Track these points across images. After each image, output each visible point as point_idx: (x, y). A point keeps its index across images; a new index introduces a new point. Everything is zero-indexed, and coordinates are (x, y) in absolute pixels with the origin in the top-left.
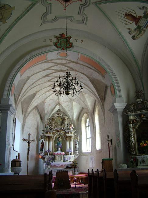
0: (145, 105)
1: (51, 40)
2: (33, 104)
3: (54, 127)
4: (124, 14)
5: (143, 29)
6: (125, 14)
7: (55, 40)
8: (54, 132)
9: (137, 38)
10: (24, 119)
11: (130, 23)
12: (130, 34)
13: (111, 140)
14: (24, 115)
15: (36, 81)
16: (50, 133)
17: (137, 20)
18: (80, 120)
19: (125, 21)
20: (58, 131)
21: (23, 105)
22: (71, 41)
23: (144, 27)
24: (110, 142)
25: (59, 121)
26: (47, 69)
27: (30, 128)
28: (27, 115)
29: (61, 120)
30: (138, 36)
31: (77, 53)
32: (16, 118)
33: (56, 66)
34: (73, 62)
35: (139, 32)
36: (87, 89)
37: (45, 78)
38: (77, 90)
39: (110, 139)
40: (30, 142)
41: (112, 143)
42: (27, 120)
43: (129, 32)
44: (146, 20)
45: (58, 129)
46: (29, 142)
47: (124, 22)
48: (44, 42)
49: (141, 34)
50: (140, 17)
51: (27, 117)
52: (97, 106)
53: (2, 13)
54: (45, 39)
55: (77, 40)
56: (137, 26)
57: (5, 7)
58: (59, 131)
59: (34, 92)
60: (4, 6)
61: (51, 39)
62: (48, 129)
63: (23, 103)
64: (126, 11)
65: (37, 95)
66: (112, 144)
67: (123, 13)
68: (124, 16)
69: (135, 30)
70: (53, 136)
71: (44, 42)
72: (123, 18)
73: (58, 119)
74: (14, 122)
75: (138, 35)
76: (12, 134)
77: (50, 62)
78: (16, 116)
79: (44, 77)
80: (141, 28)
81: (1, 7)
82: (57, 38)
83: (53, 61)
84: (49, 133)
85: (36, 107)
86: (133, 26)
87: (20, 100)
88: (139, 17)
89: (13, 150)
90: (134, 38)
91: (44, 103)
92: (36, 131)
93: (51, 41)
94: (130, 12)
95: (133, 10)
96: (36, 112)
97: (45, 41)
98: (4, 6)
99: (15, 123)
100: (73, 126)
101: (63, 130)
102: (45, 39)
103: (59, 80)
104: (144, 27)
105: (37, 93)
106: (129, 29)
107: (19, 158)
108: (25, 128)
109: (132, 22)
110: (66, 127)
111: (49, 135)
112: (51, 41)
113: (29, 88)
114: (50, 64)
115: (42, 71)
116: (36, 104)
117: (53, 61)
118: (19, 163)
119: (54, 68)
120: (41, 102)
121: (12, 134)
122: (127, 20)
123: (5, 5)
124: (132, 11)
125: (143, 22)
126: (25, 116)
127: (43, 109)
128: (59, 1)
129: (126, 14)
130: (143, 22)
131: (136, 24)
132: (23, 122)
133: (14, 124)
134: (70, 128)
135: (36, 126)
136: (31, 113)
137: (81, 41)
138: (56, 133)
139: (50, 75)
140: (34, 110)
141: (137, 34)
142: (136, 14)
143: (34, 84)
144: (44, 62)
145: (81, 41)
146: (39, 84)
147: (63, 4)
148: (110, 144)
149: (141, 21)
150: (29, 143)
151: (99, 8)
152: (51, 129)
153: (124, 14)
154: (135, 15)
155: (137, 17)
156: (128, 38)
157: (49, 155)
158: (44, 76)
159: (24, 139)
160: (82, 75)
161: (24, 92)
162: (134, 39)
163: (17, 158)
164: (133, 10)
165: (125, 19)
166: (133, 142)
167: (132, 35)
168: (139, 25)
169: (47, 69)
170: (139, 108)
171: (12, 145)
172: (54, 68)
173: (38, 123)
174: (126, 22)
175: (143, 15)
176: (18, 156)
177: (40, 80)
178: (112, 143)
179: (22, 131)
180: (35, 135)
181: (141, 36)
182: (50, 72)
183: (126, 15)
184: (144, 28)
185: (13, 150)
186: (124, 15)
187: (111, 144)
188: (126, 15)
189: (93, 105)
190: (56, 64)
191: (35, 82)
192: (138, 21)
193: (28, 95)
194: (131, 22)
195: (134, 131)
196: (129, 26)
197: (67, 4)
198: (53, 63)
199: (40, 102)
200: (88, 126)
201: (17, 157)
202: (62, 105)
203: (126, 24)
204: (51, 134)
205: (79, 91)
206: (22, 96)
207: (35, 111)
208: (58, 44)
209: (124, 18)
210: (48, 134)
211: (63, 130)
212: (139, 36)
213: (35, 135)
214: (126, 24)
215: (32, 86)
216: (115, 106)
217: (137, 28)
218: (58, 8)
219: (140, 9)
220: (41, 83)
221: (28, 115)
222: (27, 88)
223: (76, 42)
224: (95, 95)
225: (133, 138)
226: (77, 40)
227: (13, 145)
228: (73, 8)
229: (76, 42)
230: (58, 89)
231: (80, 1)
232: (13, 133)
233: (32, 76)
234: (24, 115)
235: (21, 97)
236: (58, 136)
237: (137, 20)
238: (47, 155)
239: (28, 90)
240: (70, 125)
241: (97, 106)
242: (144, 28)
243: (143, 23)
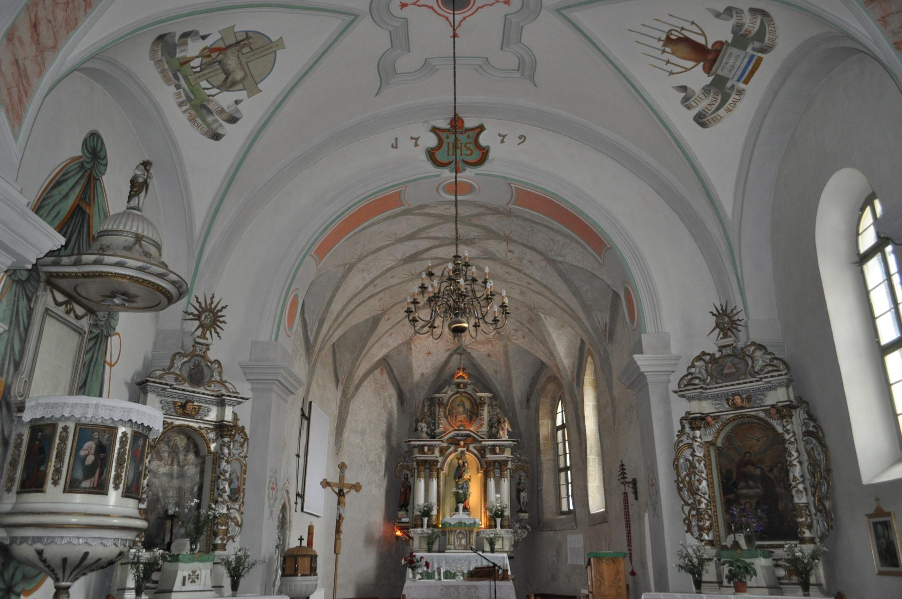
0: (750, 362)
1: (417, 139)
2: (371, 352)
3: (444, 428)
4: (659, 40)
5: (733, 86)
6: (663, 37)
7: (431, 141)
8: (445, 445)
9: (716, 120)
10: (341, 402)
11: (687, 70)
12: (689, 108)
13: (634, 482)
14: (341, 388)
15: (376, 278)
16: (431, 449)
17: (710, 57)
18: (533, 404)
19: (668, 62)
20: (457, 444)
21: (337, 356)
22: (483, 140)
23: (738, 80)
24: (630, 490)
25: (461, 409)
26: (411, 237)
27: (363, 433)
28: (352, 389)
29: (468, 405)
30: (719, 112)
31: (413, 204)
32: (311, 403)
33: (439, 224)
34: (496, 211)
35: (720, 98)
36: (551, 300)
37: (406, 267)
38: (489, 319)
39: (629, 479)
40: (345, 491)
41: (636, 493)
42: (352, 406)
43: (685, 100)
44: (742, 56)
45: (458, 435)
46: (341, 491)
47: (662, 65)
48: (393, 147)
49: (727, 105)
50: (720, 45)
51: (353, 396)
52: (590, 359)
53: (244, 61)
54: (396, 139)
55: (504, 136)
56: (711, 78)
57: (251, 41)
58: (462, 443)
59: (374, 313)
60: (248, 38)
61: (416, 136)
62: (424, 435)
63: (337, 350)
64: (667, 28)
65: (383, 320)
66: (636, 499)
67: (658, 34)
68: (664, 46)
69: (706, 90)
70: (440, 459)
71: (393, 147)
72: (658, 54)
73: (458, 402)
74: (303, 415)
75: (718, 109)
76: (298, 456)
77: (420, 214)
78: (310, 396)
79: (403, 264)
80: (729, 85)
81: (899, 12)
82: (435, 132)
83: (427, 210)
84: (426, 449)
85: (385, 363)
86: (697, 77)
87: (324, 342)
88: (716, 43)
89: (302, 510)
90: (701, 120)
91: (411, 349)
92: (385, 441)
93: (416, 145)
94: (683, 29)
95: (693, 23)
96: (386, 376)
97: (394, 146)
98: (248, 38)
99: (308, 419)
100: (507, 426)
101: (475, 440)
102: (396, 139)
103: (427, 283)
104: (738, 80)
105: (383, 314)
106: (684, 88)
107: (310, 543)
108: (346, 434)
109: (693, 64)
110: (485, 428)
111: (429, 457)
112: (416, 145)
113: (356, 301)
114: (420, 222)
115: (393, 244)
116: (384, 351)
117: (427, 210)
118: (307, 561)
119: (433, 233)
120: (400, 345)
121: (298, 456)
122: (673, 59)
123: (250, 34)
124: (687, 26)
125: (731, 62)
126: (344, 394)
127: (409, 368)
128: (431, 7)
129: (668, 38)
130: (731, 62)
131: (708, 70)
132: (340, 413)
133: (305, 422)
134: (498, 432)
135: (383, 427)
136: (366, 383)
137: (520, 137)
138: (452, 449)
139: (422, 257)
140: (377, 372)
141: (714, 107)
142: (703, 34)
143: (371, 287)
144: (396, 215)
145: (520, 137)
146: (387, 288)
147: (447, 18)
148: (631, 496)
149: (724, 61)
150: (341, 494)
151: (573, 24)
152: (433, 437)
153: (659, 40)
154: (700, 40)
155: (710, 46)
156: (682, 120)
157: (428, 526)
158: (404, 260)
159: (325, 480)
160: (530, 255)
161: (335, 314)
162: (703, 125)
163: (305, 543)
164: (693, 23)
165: (666, 56)
166: (707, 497)
167: (695, 112)
168: (719, 72)
169: (411, 237)
170: (726, 371)
171: (298, 495)
172: (433, 233)
173: (390, 414)
174: (670, 67)
175: (728, 37)
176: (305, 537)
177: (389, 275)
178: (636, 493)
179: (336, 444)
180: (380, 458)
181: (729, 110)
182: (422, 244)
183: (669, 41)
184: (735, 83)
185: (302, 510)
186: (661, 43)
187: (633, 496)
188: (669, 41)
189: (577, 352)
190: (482, 210)
191: (372, 281)
192: (714, 61)
193: (353, 321)
194: (689, 64)
195: (709, 455)
196: (681, 80)
197: (458, 18)
198: (429, 215)
199: (396, 345)
200: (563, 427)
201: (301, 539)
202: (472, 354)
203: (672, 73)
204: (433, 453)
205: (495, 321)
206: (330, 328)
207: (382, 377)
208: (441, 156)
209: (664, 51)
210: (425, 453)
211: (475, 440)
212: (722, 112)
213: (380, 458)
214: (672, 73)
215: (365, 294)
216: (639, 363)
217: (712, 84)
218: (429, 27)
219: (718, 15)
220: (395, 281)
221: (357, 388)
222: (346, 300)
223: (502, 142)
224: (577, 319)
225: (704, 483)
226: (504, 136)
227: (301, 496)
228: (482, 25)
229: (502, 142)
230: (424, 314)
231: (505, 2)
232: (302, 455)
233: (360, 259)
234: (344, 391)
235: (328, 333)
236: (458, 459)
237: (710, 57)
238: (422, 526)
239: (352, 306)
240: (499, 422)
241: (590, 359)
242: (735, 83)
243: (733, 66)
